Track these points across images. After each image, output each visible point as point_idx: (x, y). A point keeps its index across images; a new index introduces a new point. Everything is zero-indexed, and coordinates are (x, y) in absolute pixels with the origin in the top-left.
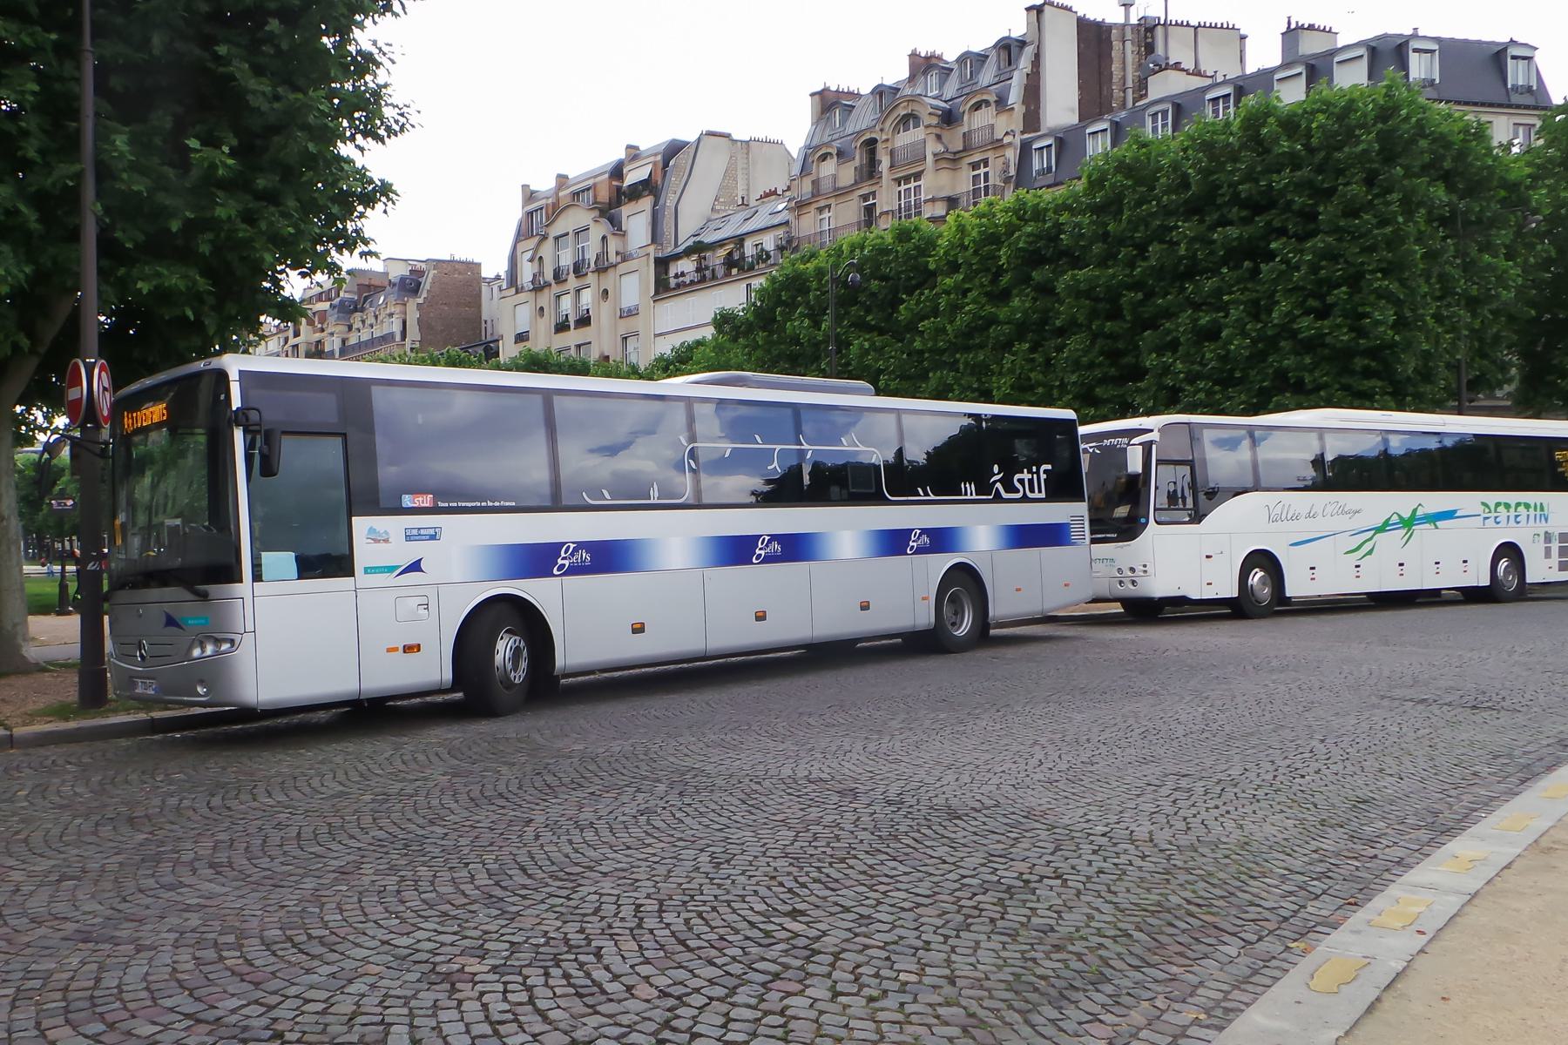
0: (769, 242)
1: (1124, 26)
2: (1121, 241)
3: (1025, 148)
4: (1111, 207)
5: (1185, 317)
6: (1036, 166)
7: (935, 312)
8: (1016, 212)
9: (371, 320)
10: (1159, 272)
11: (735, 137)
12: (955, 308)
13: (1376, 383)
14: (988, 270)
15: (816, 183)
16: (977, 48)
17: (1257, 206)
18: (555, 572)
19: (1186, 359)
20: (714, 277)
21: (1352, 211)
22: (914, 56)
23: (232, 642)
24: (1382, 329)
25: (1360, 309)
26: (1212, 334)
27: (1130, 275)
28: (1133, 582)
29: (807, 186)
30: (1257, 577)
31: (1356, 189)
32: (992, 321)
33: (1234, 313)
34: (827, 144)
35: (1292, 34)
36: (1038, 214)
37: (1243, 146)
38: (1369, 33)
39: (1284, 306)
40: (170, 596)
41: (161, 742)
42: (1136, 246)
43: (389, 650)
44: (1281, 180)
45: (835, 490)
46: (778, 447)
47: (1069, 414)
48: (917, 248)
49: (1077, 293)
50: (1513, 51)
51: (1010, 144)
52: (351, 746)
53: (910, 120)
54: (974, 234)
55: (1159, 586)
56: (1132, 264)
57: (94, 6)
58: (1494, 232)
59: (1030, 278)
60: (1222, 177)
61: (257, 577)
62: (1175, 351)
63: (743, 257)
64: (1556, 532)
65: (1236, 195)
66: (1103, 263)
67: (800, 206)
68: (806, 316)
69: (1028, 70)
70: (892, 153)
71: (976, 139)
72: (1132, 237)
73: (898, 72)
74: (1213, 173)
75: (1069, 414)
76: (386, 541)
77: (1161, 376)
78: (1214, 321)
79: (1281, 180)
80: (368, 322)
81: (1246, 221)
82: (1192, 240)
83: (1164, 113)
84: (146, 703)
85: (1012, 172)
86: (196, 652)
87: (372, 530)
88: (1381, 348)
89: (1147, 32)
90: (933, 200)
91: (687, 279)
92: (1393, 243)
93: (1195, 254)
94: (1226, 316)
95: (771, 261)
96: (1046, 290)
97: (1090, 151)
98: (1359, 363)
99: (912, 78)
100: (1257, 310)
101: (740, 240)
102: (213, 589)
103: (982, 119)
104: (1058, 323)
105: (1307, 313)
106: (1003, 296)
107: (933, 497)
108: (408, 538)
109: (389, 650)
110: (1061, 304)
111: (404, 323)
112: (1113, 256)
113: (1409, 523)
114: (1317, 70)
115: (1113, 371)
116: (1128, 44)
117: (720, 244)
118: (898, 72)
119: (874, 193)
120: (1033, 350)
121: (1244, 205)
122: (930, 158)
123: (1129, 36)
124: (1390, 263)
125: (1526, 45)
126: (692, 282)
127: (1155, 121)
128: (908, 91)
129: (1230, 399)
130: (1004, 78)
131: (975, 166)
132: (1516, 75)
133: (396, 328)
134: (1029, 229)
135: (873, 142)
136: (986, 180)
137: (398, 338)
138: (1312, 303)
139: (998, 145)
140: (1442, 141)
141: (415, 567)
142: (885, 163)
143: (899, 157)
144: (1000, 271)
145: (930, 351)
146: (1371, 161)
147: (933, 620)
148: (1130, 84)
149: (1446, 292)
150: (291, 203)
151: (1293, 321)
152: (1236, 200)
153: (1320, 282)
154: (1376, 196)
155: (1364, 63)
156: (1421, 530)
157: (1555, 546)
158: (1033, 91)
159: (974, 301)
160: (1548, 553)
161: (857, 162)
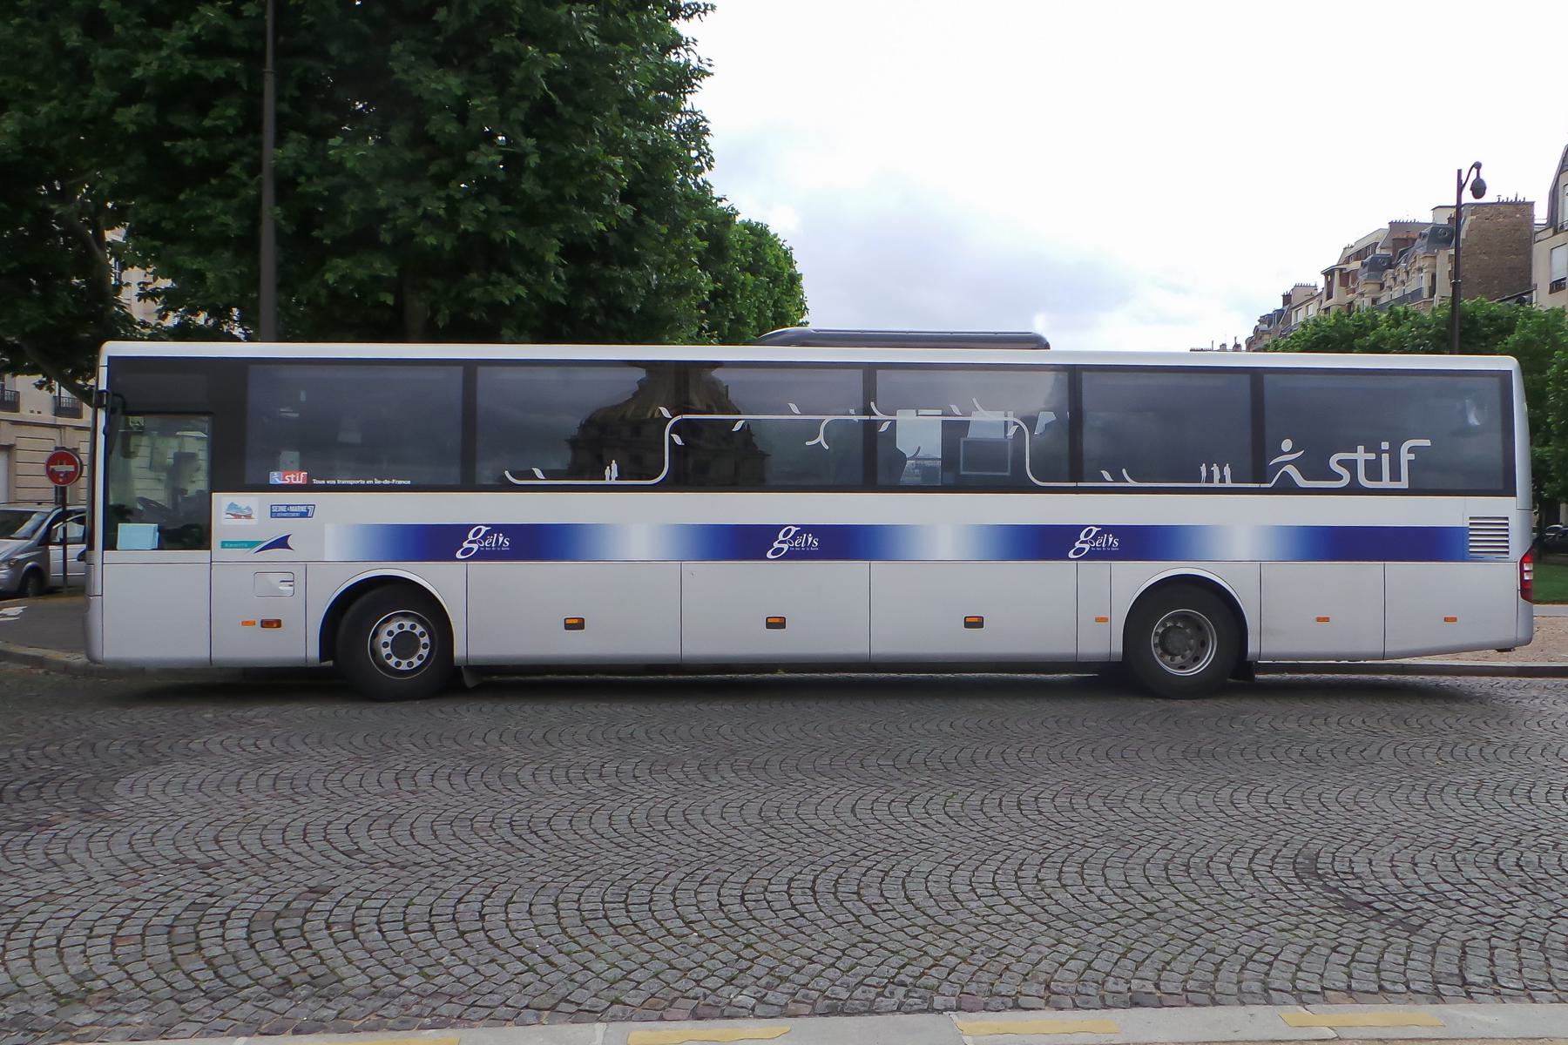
9: (1403, 277)
18: (458, 555)
43: (245, 623)
46: (828, 419)
52: (487, 706)
76: (248, 517)
80: (1399, 279)
87: (232, 506)
108: (274, 515)
109: (245, 623)
111: (1434, 277)
133: (1425, 284)
137: (1426, 294)
141: (282, 543)
147: (1118, 647)
150: (317, 187)
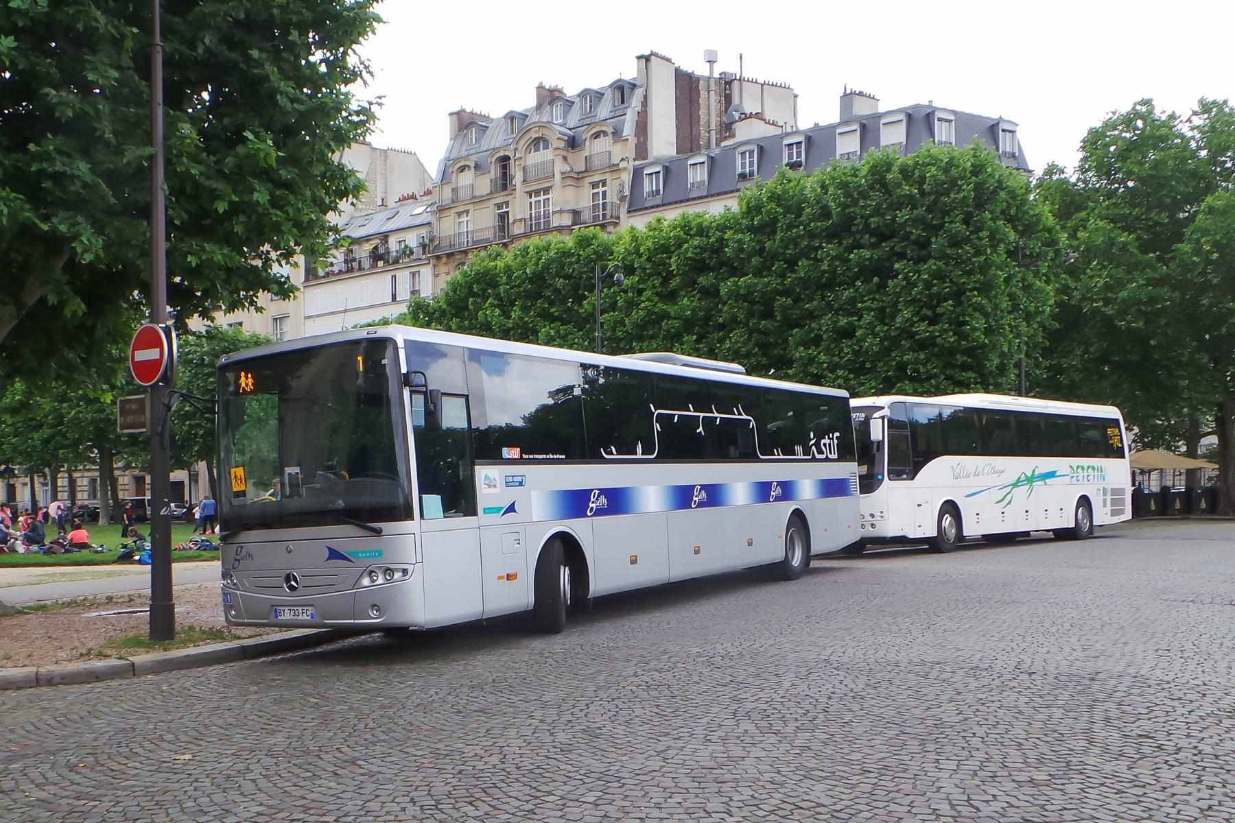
0: (412, 240)
1: (709, 78)
2: (774, 256)
3: (637, 174)
4: (768, 228)
5: (826, 320)
6: (647, 188)
7: (613, 307)
8: (683, 228)
10: (804, 282)
11: (374, 146)
12: (631, 305)
13: (971, 374)
14: (659, 274)
15: (455, 190)
16: (595, 86)
17: (882, 236)
19: (828, 351)
20: (360, 269)
21: (955, 242)
22: (540, 88)
23: (405, 571)
24: (977, 334)
25: (961, 319)
26: (848, 333)
27: (782, 284)
28: (872, 525)
29: (447, 194)
30: (947, 520)
31: (959, 227)
32: (665, 316)
33: (868, 318)
34: (467, 157)
35: (848, 98)
36: (702, 231)
37: (871, 188)
38: (907, 102)
39: (906, 314)
40: (343, 535)
41: (272, 663)
42: (786, 261)
44: (903, 215)
45: (732, 450)
46: (702, 415)
47: (843, 393)
48: (595, 253)
49: (736, 295)
50: (1003, 126)
51: (625, 169)
53: (539, 143)
54: (649, 243)
55: (891, 529)
56: (783, 276)
57: (167, 8)
58: (1040, 263)
59: (695, 282)
60: (857, 210)
61: (422, 516)
62: (818, 346)
63: (388, 252)
64: (1109, 487)
65: (867, 225)
66: (758, 273)
67: (442, 210)
68: (495, 306)
69: (639, 109)
70: (524, 169)
71: (596, 163)
72: (784, 254)
73: (526, 101)
74: (848, 207)
75: (843, 393)
77: (805, 365)
78: (850, 323)
79: (903, 215)
81: (873, 246)
82: (833, 259)
83: (751, 152)
84: (216, 635)
85: (627, 192)
86: (366, 581)
88: (974, 349)
89: (727, 83)
90: (561, 212)
91: (336, 269)
92: (985, 268)
93: (835, 270)
94: (859, 320)
95: (415, 256)
96: (711, 293)
97: (690, 180)
98: (960, 359)
99: (539, 107)
100: (884, 316)
101: (385, 237)
102: (386, 526)
103: (599, 147)
104: (721, 320)
105: (922, 320)
106: (671, 297)
107: (782, 457)
108: (508, 484)
110: (725, 304)
112: (769, 269)
113: (1030, 480)
114: (868, 129)
115: (764, 361)
116: (712, 93)
117: (366, 239)
118: (526, 101)
119: (507, 203)
120: (698, 341)
121: (873, 233)
122: (558, 176)
123: (713, 87)
124: (982, 284)
125: (1009, 121)
126: (340, 272)
127: (743, 158)
128: (536, 118)
129: (863, 384)
130: (618, 114)
131: (595, 185)
132: (1005, 144)
134: (696, 243)
135: (507, 158)
136: (604, 197)
138: (927, 312)
139: (614, 169)
140: (1013, 194)
141: (511, 509)
142: (518, 179)
143: (530, 176)
144: (671, 275)
145: (609, 339)
146: (968, 206)
148: (713, 126)
149: (1015, 308)
151: (912, 325)
152: (867, 228)
153: (931, 296)
154: (972, 233)
155: (904, 123)
156: (1038, 485)
157: (1109, 498)
158: (642, 127)
159: (648, 300)
160: (1105, 505)
161: (492, 175)
